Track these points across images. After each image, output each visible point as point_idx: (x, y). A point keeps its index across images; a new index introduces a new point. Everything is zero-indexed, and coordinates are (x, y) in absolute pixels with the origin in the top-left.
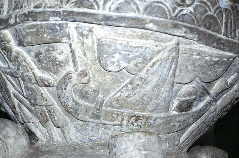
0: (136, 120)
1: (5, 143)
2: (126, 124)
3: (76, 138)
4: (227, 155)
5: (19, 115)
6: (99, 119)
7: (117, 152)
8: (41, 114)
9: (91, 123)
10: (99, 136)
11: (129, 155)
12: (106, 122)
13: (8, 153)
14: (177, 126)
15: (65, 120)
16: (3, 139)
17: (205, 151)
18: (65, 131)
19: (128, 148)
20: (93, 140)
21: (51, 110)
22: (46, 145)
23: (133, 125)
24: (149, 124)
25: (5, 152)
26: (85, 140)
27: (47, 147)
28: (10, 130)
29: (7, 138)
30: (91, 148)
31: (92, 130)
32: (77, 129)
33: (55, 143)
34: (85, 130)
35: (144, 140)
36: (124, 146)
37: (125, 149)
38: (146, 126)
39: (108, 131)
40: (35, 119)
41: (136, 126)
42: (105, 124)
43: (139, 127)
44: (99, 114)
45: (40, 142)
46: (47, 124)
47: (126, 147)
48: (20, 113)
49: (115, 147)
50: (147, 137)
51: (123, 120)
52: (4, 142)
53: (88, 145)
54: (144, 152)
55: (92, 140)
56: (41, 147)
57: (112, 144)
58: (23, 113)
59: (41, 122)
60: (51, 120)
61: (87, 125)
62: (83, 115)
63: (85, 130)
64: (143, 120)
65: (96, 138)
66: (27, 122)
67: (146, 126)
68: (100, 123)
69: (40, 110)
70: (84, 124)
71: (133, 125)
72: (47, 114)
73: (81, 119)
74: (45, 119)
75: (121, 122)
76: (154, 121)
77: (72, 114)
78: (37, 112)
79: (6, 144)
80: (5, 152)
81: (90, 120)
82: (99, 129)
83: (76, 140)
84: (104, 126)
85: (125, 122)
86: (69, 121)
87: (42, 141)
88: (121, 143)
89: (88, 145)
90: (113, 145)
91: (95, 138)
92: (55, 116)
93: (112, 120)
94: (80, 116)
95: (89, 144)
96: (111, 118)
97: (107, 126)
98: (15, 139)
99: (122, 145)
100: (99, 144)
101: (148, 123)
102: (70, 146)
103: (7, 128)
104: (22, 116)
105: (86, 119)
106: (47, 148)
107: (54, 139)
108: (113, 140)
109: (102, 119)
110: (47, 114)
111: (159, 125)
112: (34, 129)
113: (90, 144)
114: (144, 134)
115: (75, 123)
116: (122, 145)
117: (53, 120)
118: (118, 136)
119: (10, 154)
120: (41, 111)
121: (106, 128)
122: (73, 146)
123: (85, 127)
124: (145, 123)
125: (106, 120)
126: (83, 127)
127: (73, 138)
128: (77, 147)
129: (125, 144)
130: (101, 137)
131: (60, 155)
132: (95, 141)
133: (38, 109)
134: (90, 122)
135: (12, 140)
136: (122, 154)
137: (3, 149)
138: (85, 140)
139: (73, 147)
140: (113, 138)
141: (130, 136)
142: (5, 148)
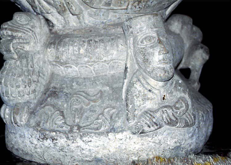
0: (138, 4)
1: (34, 32)
2: (130, 7)
3: (89, 22)
4: (192, 20)
5: (38, 8)
6: (110, 6)
7: (133, 31)
8: (60, 6)
9: (103, 10)
10: (109, 18)
11: (144, 33)
12: (115, 8)
13: (37, 39)
14: (166, 4)
15: (81, 10)
16: (32, 29)
17: (176, 19)
18: (81, 18)
19: (142, 28)
20: (104, 22)
21: (70, 3)
22: (63, 29)
23: (136, 8)
24: (148, 6)
25: (35, 39)
26: (97, 23)
27: (64, 31)
28: (35, 21)
29: (34, 28)
30: (104, 29)
31: (103, 15)
32: (90, 15)
33: (71, 28)
34: (98, 15)
35: (153, 20)
36: (139, 26)
37: (140, 28)
38: (145, 7)
39: (116, 14)
40: (54, 11)
41: (138, 9)
42: (114, 9)
43: (140, 9)
44: (110, 3)
45: (57, 28)
46: (64, 13)
47: (141, 27)
48: (39, 6)
49: (131, 27)
50: (155, 18)
51: (128, 5)
52: (33, 31)
53: (100, 26)
54: (155, 29)
55: (103, 23)
56: (58, 31)
57: (128, 26)
58: (42, 6)
59: (59, 13)
60: (68, 10)
61: (100, 11)
62: (98, 4)
63: (98, 15)
64: (143, 4)
65: (106, 20)
66: (45, 12)
67: (145, 7)
68: (110, 9)
69: (60, 3)
70: (96, 11)
71: (136, 8)
72: (65, 5)
73: (96, 7)
74: (64, 9)
75: (127, 7)
76: (151, 3)
77: (88, 4)
78: (56, 5)
79: (35, 33)
80: (35, 39)
81: (102, 7)
82: (109, 13)
83: (89, 24)
84: (113, 11)
85: (130, 7)
86: (83, 9)
87: (59, 27)
88: (136, 24)
89: (100, 26)
90: (129, 26)
91: (106, 21)
92: (73, 7)
93: (120, 6)
94: (94, 5)
95: (100, 25)
96: (119, 4)
97: (115, 11)
98: (41, 28)
99: (138, 25)
100: (109, 25)
101: (146, 5)
102: (85, 28)
103: (33, 20)
104: (40, 9)
105: (100, 7)
106: (64, 32)
107: (70, 24)
108: (129, 22)
109: (111, 6)
110: (65, 5)
111: (154, 6)
112: (50, 17)
113: (102, 26)
114: (153, 15)
115: (89, 10)
116: (137, 25)
117: (71, 10)
118: (133, 19)
119: (38, 40)
120: (60, 4)
121: (115, 12)
122: (88, 28)
123: (98, 13)
124: (145, 5)
125: (115, 6)
126: (96, 13)
127: (87, 22)
128: (92, 29)
129: (139, 25)
130: (110, 19)
131: (80, 36)
132: (106, 23)
133: (57, 2)
134: (102, 9)
135: (39, 29)
136: (138, 33)
137: (33, 37)
138: (97, 23)
139: (89, 29)
140: (129, 21)
141: (143, 18)
142: (35, 36)
